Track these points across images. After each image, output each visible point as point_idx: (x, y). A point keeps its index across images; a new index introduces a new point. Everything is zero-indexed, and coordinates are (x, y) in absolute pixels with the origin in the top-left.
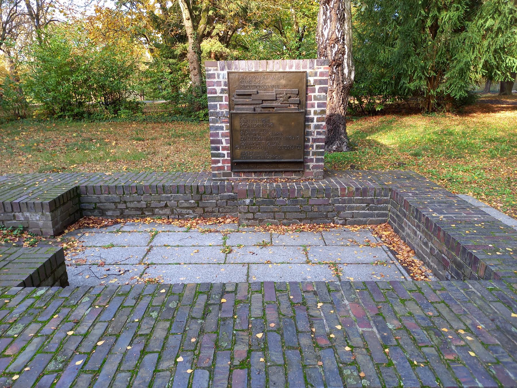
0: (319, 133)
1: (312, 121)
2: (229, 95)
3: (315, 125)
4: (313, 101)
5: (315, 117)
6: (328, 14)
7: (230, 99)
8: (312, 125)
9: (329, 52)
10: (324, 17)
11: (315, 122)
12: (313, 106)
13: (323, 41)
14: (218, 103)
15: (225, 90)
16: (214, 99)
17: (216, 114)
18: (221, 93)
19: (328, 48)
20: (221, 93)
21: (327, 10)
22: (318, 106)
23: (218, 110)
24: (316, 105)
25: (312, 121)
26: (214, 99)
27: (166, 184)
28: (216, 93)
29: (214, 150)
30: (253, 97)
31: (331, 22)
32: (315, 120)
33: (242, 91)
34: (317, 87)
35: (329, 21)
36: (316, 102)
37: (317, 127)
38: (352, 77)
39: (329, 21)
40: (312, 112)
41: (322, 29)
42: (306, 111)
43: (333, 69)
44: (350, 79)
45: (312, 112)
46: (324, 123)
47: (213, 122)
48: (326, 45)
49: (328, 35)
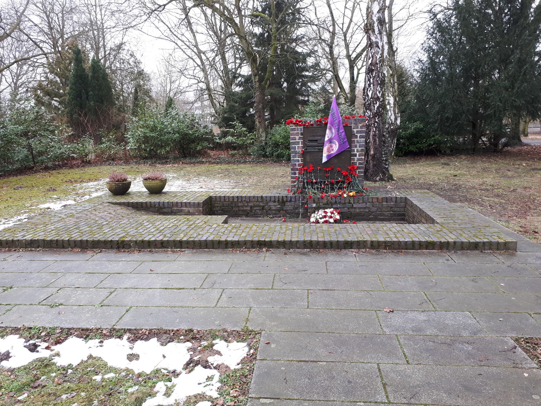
0: (360, 164)
1: (356, 156)
2: (304, 141)
3: (358, 158)
4: (356, 144)
5: (358, 154)
6: (372, 80)
7: (303, 143)
8: (356, 158)
10: (369, 83)
11: (358, 157)
12: (356, 147)
13: (368, 99)
14: (297, 146)
15: (301, 137)
16: (294, 143)
17: (296, 153)
18: (298, 139)
19: (372, 104)
20: (298, 139)
21: (371, 77)
22: (359, 147)
23: (297, 150)
24: (358, 146)
25: (356, 156)
26: (294, 143)
27: (264, 195)
28: (296, 140)
29: (293, 174)
30: (319, 142)
31: (373, 86)
32: (358, 155)
33: (311, 138)
34: (359, 135)
35: (372, 85)
36: (358, 144)
37: (358, 160)
38: (398, 122)
39: (372, 85)
40: (356, 150)
41: (367, 91)
42: (351, 149)
43: (375, 119)
44: (396, 124)
45: (356, 150)
46: (363, 157)
47: (293, 157)
48: (370, 102)
49: (372, 95)
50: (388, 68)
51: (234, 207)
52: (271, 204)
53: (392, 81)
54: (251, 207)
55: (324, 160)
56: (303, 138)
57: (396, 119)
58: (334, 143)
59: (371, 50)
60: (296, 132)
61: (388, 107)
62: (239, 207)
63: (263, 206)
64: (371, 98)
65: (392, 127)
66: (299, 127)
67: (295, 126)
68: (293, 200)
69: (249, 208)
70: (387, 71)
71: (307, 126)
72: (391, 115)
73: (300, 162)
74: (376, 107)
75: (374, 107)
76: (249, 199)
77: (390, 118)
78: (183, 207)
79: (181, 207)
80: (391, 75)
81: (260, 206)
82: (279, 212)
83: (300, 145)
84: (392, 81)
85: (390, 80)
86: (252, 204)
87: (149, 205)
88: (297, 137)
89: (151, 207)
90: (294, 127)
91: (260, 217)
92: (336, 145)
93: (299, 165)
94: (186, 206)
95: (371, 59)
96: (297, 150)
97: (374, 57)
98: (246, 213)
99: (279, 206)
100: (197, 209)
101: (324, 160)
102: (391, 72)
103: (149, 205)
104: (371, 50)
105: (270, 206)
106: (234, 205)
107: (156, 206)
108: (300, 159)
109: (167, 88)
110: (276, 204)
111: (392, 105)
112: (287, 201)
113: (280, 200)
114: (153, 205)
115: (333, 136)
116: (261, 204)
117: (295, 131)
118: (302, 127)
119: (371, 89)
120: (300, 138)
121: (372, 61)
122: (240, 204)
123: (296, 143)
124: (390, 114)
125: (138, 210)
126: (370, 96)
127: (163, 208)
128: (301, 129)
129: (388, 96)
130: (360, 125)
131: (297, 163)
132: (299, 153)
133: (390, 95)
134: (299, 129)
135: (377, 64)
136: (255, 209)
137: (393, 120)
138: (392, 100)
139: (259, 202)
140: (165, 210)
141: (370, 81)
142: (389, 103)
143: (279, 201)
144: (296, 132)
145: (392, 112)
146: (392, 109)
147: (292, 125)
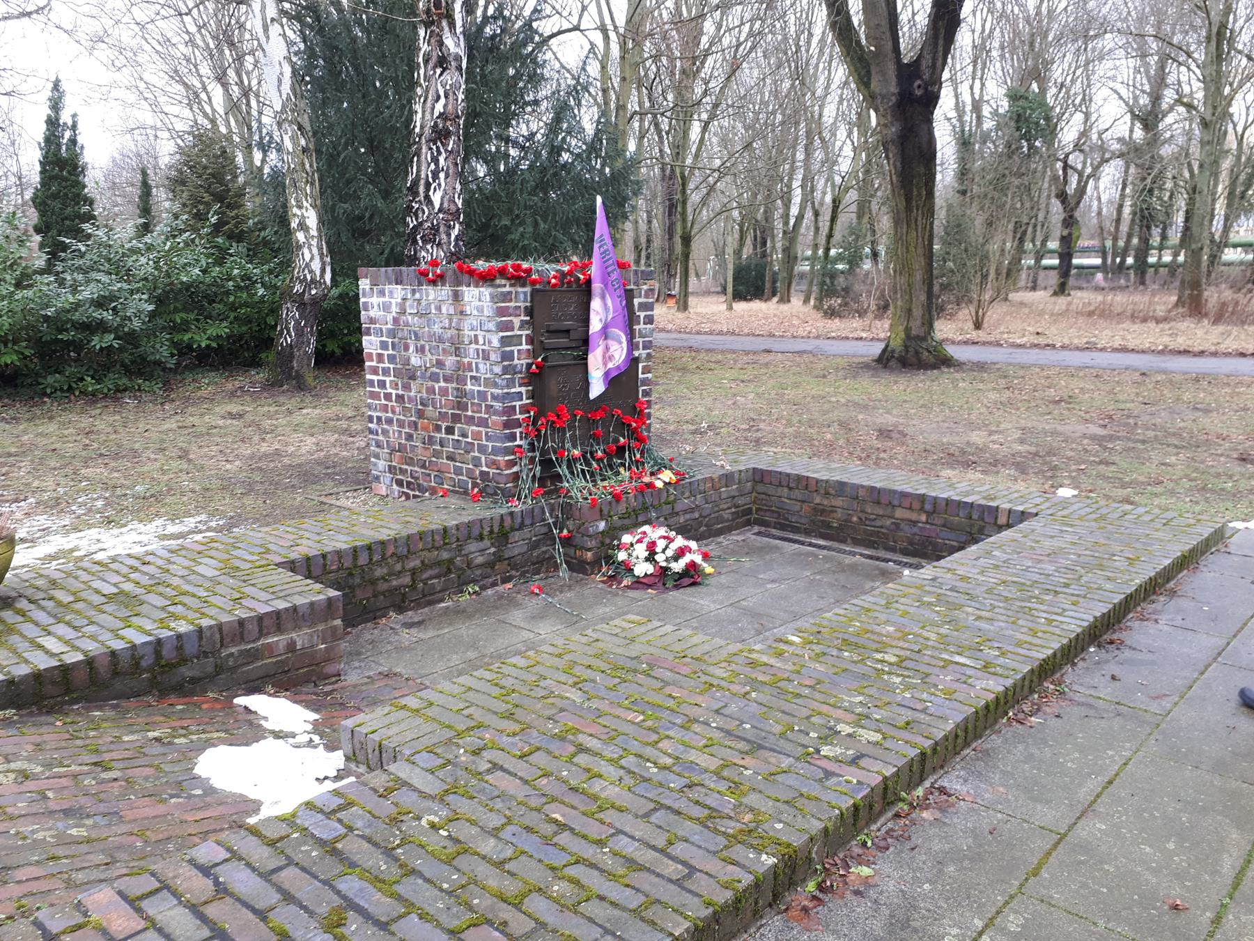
9: (444, 236)
10: (433, 166)
14: (515, 349)
18: (521, 328)
20: (521, 328)
33: (555, 325)
35: (442, 175)
36: (641, 340)
39: (442, 175)
50: (293, 131)
51: (359, 585)
52: (473, 547)
53: (307, 166)
54: (414, 572)
55: (597, 388)
56: (531, 324)
57: (323, 271)
58: (613, 339)
59: (441, 75)
60: (512, 304)
61: (300, 236)
62: (373, 582)
63: (451, 561)
64: (440, 210)
65: (313, 292)
66: (520, 290)
67: (511, 285)
68: (528, 522)
69: (407, 580)
70: (292, 138)
71: (555, 285)
72: (312, 259)
73: (525, 401)
74: (453, 237)
75: (449, 235)
76: (408, 545)
77: (308, 265)
78: (268, 634)
79: (261, 634)
80: (304, 150)
81: (439, 563)
82: (493, 568)
83: (525, 347)
84: (307, 166)
85: (303, 164)
86: (417, 563)
87: (103, 668)
88: (517, 322)
89: (116, 673)
90: (508, 289)
91: (442, 600)
92: (620, 343)
93: (525, 409)
94: (279, 629)
95: (442, 101)
96: (516, 361)
97: (451, 97)
98: (398, 600)
99: (493, 550)
100: (321, 627)
101: (597, 388)
102: (303, 142)
103: (103, 668)
104: (441, 75)
105: (467, 555)
106: (357, 580)
107: (144, 664)
108: (523, 389)
109: (826, 112)
110: (487, 543)
111: (314, 232)
112: (513, 529)
113: (496, 530)
114: (125, 662)
115: (610, 316)
116: (445, 555)
117: (511, 300)
118: (528, 289)
119: (439, 185)
120: (523, 324)
121: (445, 106)
122: (379, 572)
123: (515, 340)
124: (307, 257)
125: (50, 711)
126: (437, 206)
127: (179, 664)
128: (525, 293)
129: (300, 207)
130: (645, 287)
131: (518, 404)
132: (521, 372)
133: (305, 204)
134: (522, 297)
135: (458, 117)
136: (424, 576)
137: (318, 273)
138: (312, 219)
139: (437, 549)
140: (187, 672)
141: (437, 164)
142: (303, 226)
143: (491, 532)
144: (512, 304)
145: (315, 251)
146: (314, 242)
147: (503, 282)
